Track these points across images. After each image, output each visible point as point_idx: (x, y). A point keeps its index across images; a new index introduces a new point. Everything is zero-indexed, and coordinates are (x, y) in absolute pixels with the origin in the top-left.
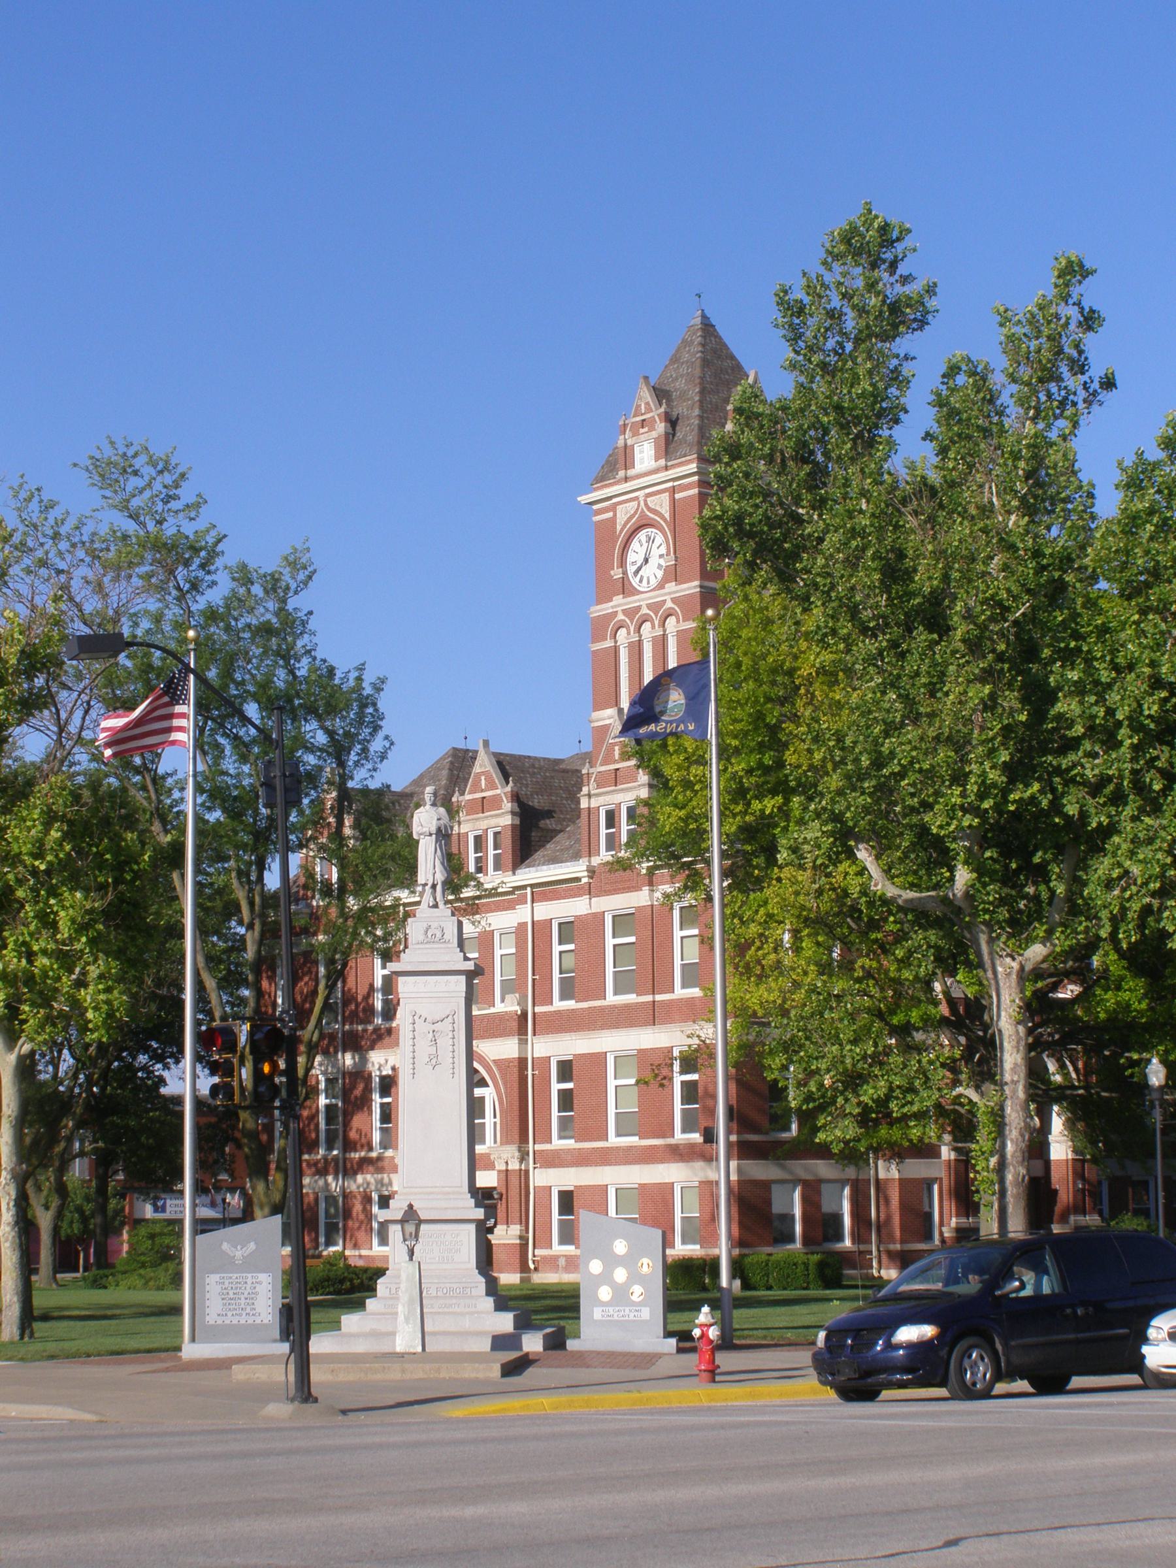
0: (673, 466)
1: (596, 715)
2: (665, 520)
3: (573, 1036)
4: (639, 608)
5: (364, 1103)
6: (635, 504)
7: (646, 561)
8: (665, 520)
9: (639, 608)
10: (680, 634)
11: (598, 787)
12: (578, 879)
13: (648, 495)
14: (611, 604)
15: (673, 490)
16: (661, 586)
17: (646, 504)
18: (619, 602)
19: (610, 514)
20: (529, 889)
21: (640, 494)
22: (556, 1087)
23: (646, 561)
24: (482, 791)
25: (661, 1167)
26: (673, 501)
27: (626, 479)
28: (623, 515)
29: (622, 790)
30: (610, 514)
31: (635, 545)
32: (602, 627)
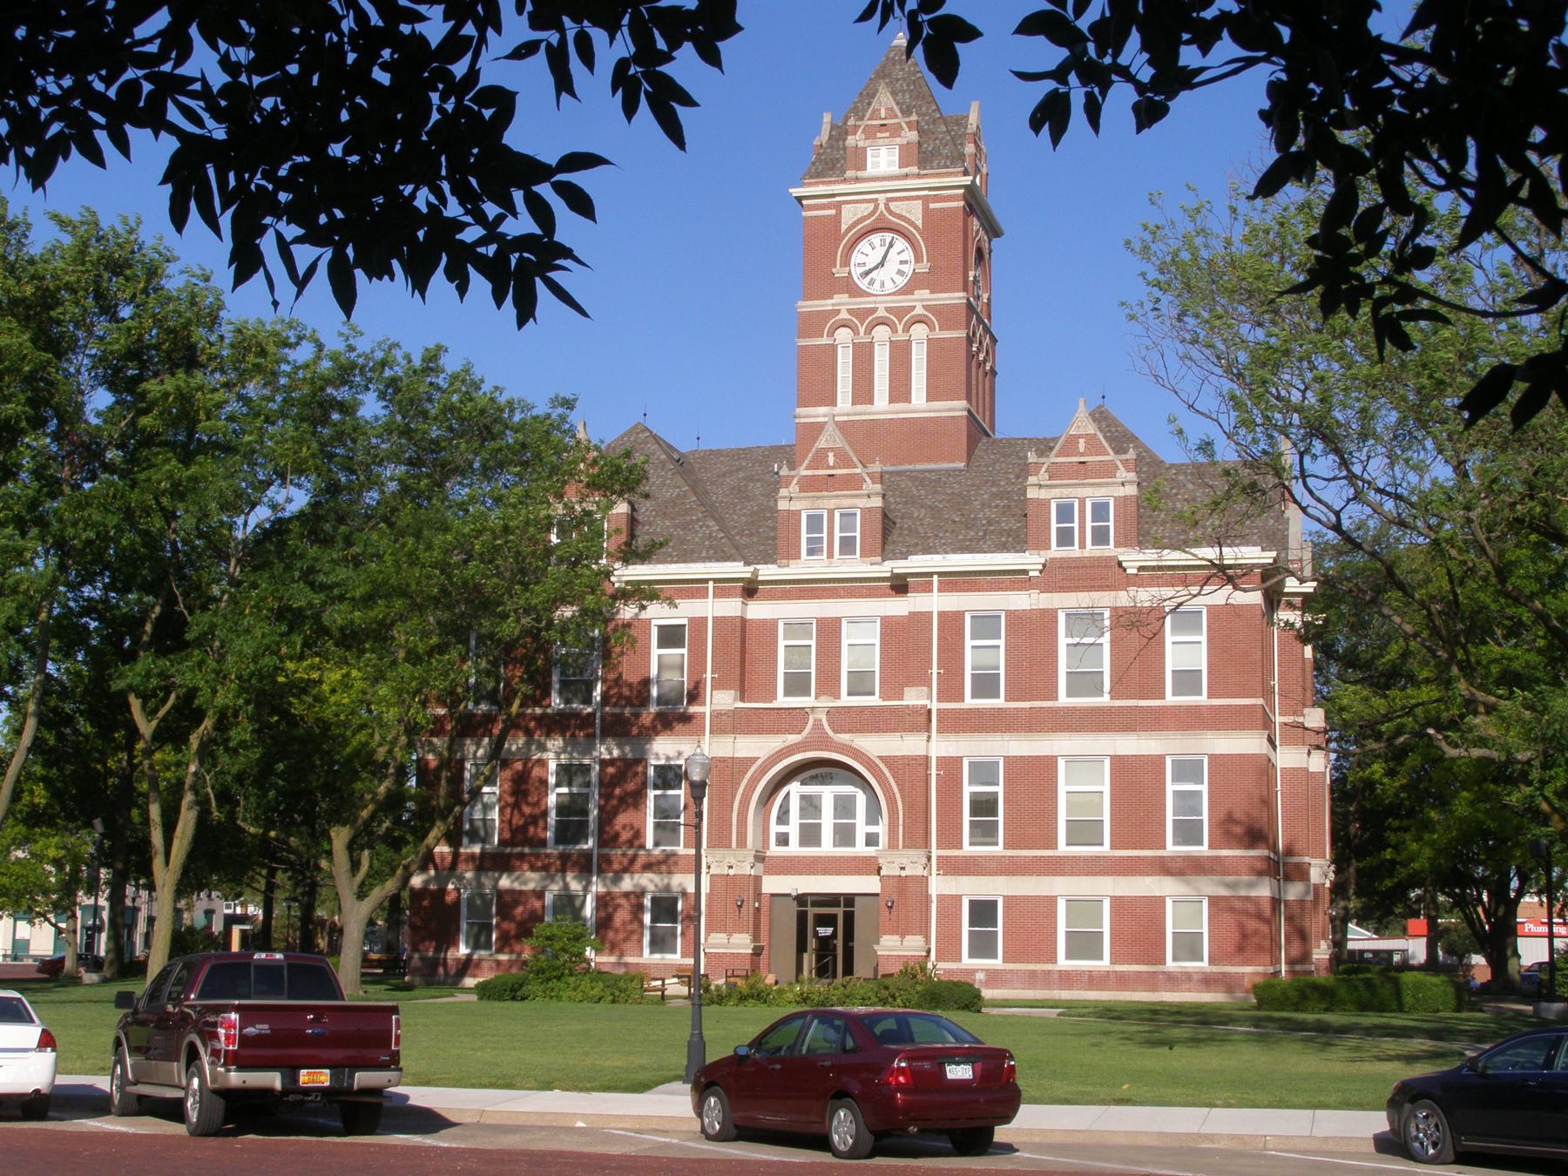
0: (926, 176)
1: (801, 411)
2: (916, 227)
3: (1007, 736)
4: (875, 310)
5: (637, 798)
6: (871, 206)
7: (882, 264)
8: (916, 227)
9: (875, 310)
10: (934, 346)
11: (1050, 478)
12: (1025, 572)
13: (889, 200)
14: (830, 302)
15: (926, 200)
16: (907, 290)
17: (887, 208)
18: (841, 301)
19: (833, 212)
20: (935, 578)
21: (882, 197)
22: (968, 790)
23: (882, 264)
24: (829, 468)
25: (1148, 880)
26: (926, 209)
27: (857, 180)
28: (849, 215)
29: (1093, 485)
30: (833, 212)
31: (864, 245)
32: (814, 324)
